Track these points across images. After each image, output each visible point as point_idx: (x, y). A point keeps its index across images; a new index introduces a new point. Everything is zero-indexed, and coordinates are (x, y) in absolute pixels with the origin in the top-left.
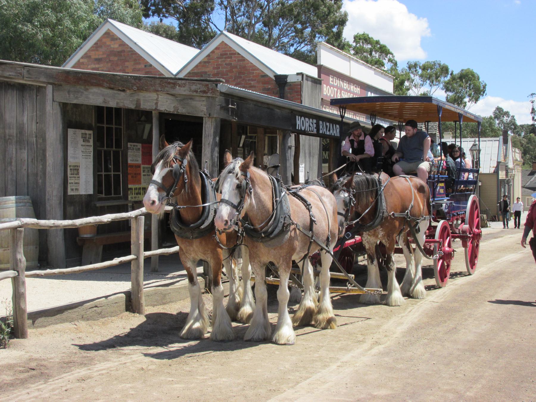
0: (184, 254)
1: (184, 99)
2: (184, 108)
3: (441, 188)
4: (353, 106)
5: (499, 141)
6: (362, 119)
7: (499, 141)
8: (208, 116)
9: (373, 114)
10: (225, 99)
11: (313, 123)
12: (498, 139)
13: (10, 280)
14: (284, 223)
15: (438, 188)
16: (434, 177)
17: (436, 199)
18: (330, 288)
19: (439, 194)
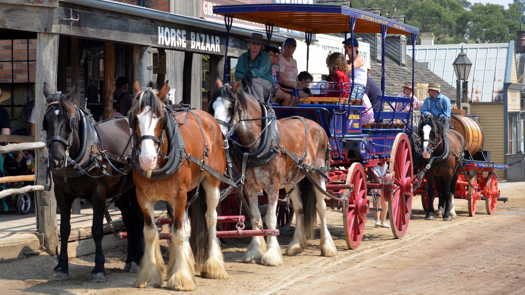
0: (143, 194)
1: (11, 10)
2: (12, 21)
3: (355, 121)
4: (243, 14)
5: (508, 48)
6: (259, 28)
7: (508, 48)
8: (43, 31)
9: (270, 23)
10: (65, 9)
11: (181, 36)
12: (506, 45)
13: (306, 71)
14: (271, 146)
15: (352, 121)
16: (344, 107)
17: (346, 136)
18: (218, 236)
19: (352, 128)
